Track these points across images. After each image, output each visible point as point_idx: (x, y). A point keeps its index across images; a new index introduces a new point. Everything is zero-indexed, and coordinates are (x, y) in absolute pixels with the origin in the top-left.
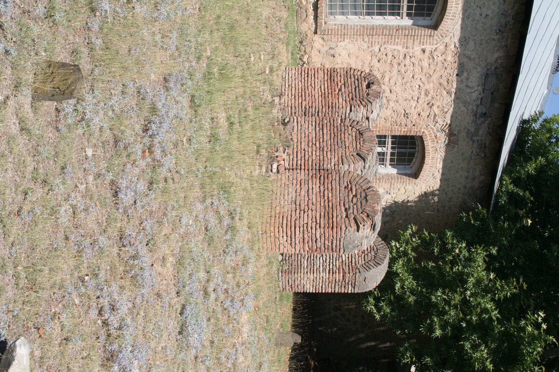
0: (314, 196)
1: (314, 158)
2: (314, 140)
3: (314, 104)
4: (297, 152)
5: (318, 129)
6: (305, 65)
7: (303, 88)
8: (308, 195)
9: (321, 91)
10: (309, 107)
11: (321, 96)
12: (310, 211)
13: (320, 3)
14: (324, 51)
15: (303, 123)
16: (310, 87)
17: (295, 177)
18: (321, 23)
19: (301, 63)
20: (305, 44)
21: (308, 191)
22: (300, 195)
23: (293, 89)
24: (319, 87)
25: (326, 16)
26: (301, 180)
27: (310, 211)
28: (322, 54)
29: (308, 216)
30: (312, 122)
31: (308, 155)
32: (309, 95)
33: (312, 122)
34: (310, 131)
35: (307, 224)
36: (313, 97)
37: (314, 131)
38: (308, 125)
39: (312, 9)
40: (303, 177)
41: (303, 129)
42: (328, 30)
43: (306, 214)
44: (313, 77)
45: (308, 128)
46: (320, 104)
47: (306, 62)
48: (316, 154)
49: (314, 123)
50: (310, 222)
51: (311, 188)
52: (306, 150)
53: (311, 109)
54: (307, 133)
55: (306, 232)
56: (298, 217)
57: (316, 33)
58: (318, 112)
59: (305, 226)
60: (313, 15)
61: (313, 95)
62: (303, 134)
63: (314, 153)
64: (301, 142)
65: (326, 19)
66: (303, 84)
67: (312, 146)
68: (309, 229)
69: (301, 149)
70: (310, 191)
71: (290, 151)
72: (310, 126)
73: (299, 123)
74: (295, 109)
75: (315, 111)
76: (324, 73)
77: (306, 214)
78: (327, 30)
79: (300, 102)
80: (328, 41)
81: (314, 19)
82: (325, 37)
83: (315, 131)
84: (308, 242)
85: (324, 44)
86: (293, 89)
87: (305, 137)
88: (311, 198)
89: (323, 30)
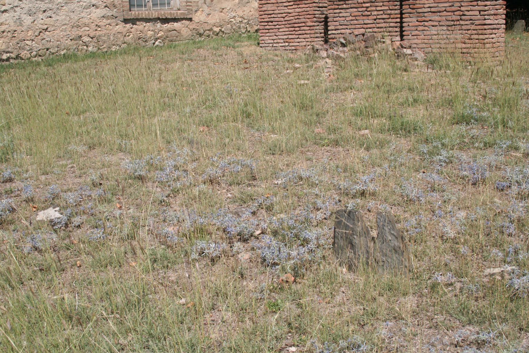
0: (440, 5)
1: (387, 8)
2: (360, 9)
3: (310, 13)
4: (378, 28)
5: (345, 6)
6: (223, 30)
7: (288, 26)
8: (440, 12)
9: (292, 5)
10: (315, 17)
11: (298, 5)
12: (462, 9)
13: (161, 16)
14: (209, 10)
15: (337, 23)
16: (286, 19)
17: (413, 28)
18: (181, 14)
19: (221, 34)
20: (202, 31)
21: (434, 12)
22: (440, 22)
23: (290, 37)
24: (286, 8)
25: (171, 9)
26: (417, 21)
27: (462, 9)
28: (211, 12)
29: (469, 11)
30: (335, 13)
31: (382, 15)
32: (298, 19)
33: (335, 13)
34: (348, 14)
35: (480, 11)
36: (300, 14)
37: (348, 10)
38: (340, 17)
39: (167, 25)
40: (414, 19)
41: (345, 23)
42: (187, 6)
43: (466, 13)
44: (273, 16)
45: (344, 17)
46: (311, 5)
47: (220, 28)
48: (381, 6)
49: (338, 11)
50: (477, 8)
51: (429, 10)
52: (375, 17)
53: (317, 16)
54: (351, 18)
55: (489, 12)
56: (471, 21)
57: (190, 20)
58: (319, 7)
59: (482, 13)
60: (173, 23)
61: (297, 14)
62: (352, 22)
63: (378, 8)
64: (365, 24)
65: (174, 9)
66: (283, 26)
67: (369, 11)
68: (486, 8)
69: (374, 23)
70: (433, 10)
71: (379, 35)
72: (341, 15)
73: (337, 27)
74: (317, 33)
75: (318, 11)
76: (266, 4)
77: (466, 13)
78: (188, 7)
79: (308, 28)
80: (198, 6)
81: (177, 22)
82: (194, 9)
83: (348, 9)
84: (497, 10)
85: (201, 10)
86: (290, 37)
87: (357, 20)
88: (444, 9)
89: (188, 12)
